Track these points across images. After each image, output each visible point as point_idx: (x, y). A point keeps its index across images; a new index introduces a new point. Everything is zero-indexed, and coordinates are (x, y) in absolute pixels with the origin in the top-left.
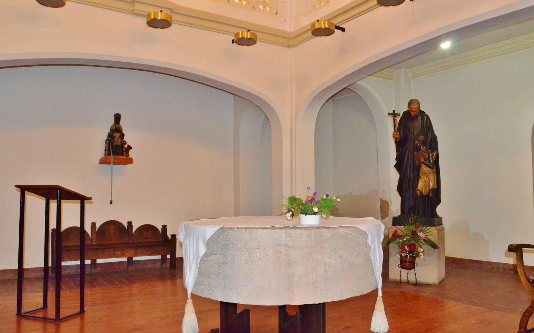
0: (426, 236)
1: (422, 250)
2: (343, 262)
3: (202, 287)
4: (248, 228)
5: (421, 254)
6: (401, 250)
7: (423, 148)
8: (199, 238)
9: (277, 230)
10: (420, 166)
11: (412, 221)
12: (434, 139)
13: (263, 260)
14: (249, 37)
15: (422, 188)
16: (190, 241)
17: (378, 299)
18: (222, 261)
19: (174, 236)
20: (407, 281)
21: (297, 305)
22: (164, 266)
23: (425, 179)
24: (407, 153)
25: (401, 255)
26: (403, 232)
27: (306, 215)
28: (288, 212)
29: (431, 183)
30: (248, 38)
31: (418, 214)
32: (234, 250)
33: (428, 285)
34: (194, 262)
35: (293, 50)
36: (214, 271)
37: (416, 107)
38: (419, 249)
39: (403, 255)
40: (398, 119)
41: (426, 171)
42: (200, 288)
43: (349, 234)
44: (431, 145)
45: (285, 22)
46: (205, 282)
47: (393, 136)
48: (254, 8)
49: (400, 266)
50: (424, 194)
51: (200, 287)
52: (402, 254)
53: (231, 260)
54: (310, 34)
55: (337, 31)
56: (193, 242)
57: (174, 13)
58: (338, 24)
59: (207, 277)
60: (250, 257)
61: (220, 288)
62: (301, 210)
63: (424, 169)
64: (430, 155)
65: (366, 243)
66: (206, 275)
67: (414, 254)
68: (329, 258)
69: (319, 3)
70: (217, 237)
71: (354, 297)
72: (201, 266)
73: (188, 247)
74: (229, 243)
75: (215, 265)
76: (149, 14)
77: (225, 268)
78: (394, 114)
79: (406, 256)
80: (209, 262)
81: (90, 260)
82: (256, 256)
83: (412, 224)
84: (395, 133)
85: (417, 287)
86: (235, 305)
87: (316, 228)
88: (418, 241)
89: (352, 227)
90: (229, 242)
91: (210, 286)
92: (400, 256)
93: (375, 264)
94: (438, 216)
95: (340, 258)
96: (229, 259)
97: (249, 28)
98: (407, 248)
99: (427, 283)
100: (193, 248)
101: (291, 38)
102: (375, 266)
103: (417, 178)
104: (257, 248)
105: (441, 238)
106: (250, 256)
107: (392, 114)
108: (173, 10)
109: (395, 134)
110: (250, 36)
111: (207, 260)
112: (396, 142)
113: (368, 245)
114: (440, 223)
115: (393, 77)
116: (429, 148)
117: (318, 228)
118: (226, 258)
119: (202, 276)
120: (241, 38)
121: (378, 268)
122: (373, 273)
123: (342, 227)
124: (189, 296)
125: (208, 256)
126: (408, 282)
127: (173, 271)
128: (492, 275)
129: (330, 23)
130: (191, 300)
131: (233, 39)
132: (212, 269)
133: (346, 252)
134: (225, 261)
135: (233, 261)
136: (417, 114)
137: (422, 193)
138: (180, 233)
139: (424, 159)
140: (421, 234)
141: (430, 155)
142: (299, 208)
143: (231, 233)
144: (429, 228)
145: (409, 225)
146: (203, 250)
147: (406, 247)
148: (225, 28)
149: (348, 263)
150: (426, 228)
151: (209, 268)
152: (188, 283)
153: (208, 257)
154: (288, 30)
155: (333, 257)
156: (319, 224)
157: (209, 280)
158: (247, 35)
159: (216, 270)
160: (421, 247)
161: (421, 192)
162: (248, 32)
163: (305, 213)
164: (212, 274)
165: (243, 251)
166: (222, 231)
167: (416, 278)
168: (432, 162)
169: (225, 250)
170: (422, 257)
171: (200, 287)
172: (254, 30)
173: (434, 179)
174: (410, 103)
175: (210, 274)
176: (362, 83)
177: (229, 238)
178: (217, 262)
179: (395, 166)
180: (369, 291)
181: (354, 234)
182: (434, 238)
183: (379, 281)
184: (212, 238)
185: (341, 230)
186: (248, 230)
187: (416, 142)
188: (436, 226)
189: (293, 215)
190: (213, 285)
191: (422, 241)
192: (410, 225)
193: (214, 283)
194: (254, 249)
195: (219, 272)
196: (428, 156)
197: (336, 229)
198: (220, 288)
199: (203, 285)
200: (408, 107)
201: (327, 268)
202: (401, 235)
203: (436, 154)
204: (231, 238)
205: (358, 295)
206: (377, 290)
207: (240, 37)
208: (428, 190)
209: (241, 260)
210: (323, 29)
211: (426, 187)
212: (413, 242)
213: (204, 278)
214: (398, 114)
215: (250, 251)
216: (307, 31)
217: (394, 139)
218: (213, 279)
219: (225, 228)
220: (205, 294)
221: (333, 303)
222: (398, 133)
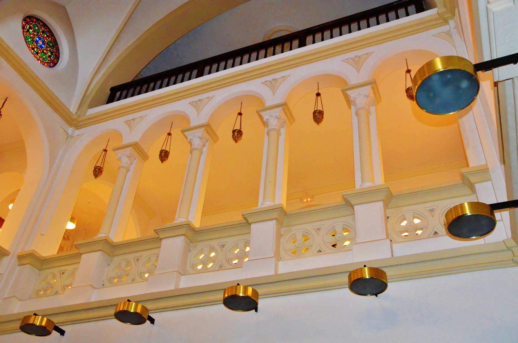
21: (326, 41)
55: (55, 333)
81: (494, 211)
128: (333, 227)
148: (330, 281)
210: (130, 312)
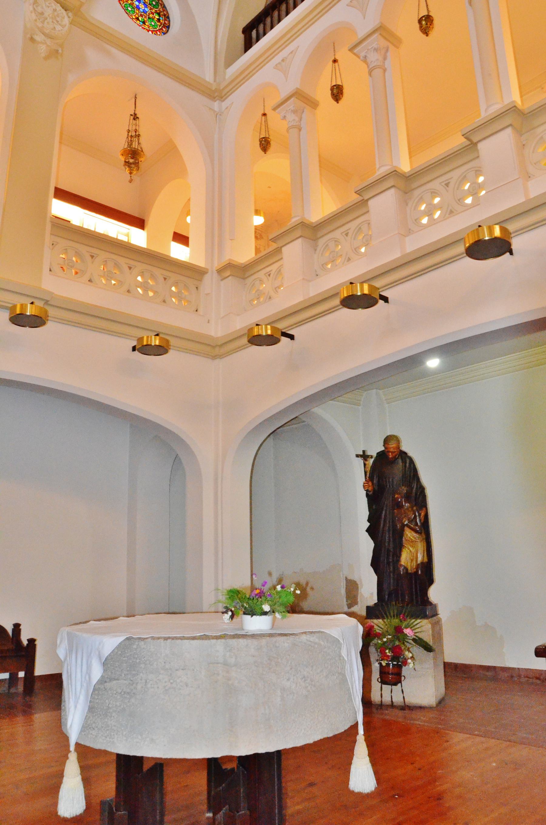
0: (415, 633)
1: (410, 655)
2: (307, 685)
3: (94, 733)
4: (169, 638)
5: (409, 661)
6: (380, 656)
7: (406, 505)
8: (92, 655)
9: (212, 640)
10: (402, 530)
11: (394, 612)
12: (421, 490)
13: (192, 687)
14: (157, 343)
15: (406, 562)
16: (76, 658)
17: (358, 740)
18: (128, 690)
19: (32, 642)
20: (391, 703)
22: (13, 690)
23: (411, 549)
24: (384, 512)
25: (380, 664)
26: (382, 628)
27: (252, 616)
28: (226, 612)
29: (419, 555)
30: (155, 345)
31: (403, 601)
32: (146, 672)
33: (421, 708)
34: (83, 692)
35: (221, 363)
36: (114, 706)
37: (394, 445)
38: (407, 653)
39: (384, 663)
40: (371, 461)
41: (412, 538)
42: (91, 734)
43: (315, 643)
44: (416, 499)
45: (209, 322)
46: (100, 723)
47: (364, 488)
48: (164, 301)
49: (379, 680)
50: (410, 571)
51: (91, 732)
52: (382, 662)
53: (142, 687)
54: (245, 340)
55: (284, 339)
56: (82, 660)
57: (50, 305)
58: (285, 329)
59: (103, 715)
60: (171, 683)
61: (124, 733)
62: (245, 608)
63: (409, 535)
64: (417, 514)
65: (340, 656)
66: (101, 713)
67: (399, 662)
68: (288, 680)
69: (258, 299)
70: (120, 652)
71: (325, 739)
72: (94, 698)
73: (73, 668)
74: (140, 662)
75: (116, 696)
76: (15, 306)
77: (133, 700)
78: (364, 456)
79: (388, 665)
80: (107, 692)
82: (181, 681)
83: (394, 616)
84: (366, 483)
85: (407, 712)
86: (141, 758)
87: (269, 636)
88: (404, 642)
89: (319, 632)
90: (139, 661)
91: (107, 730)
92: (379, 665)
93: (352, 686)
94: (431, 604)
95: (304, 679)
96: (139, 687)
97: (159, 330)
98: (389, 652)
99: (419, 705)
100: (82, 670)
101: (217, 345)
102: (352, 688)
103: (399, 547)
104: (182, 669)
105: (438, 635)
106: (171, 681)
107: (361, 456)
108: (48, 301)
109: (366, 484)
110: (159, 342)
111: (104, 688)
112: (367, 495)
113: (342, 658)
114: (435, 614)
115: (360, 401)
116: (414, 503)
117: (271, 635)
118: (134, 685)
119: (94, 715)
120: (146, 345)
121: (357, 692)
122: (350, 699)
123: (305, 633)
124: (72, 748)
125: (106, 682)
126: (392, 705)
127: (28, 698)
129: (273, 328)
130: (76, 754)
131: (77, 275)
132: (111, 702)
133: (312, 670)
134: (132, 690)
135: (145, 690)
136: (396, 455)
137: (407, 569)
138: (59, 646)
139: (408, 520)
140: (407, 631)
141: (417, 514)
142: (243, 606)
143: (143, 647)
144: (419, 621)
145: (390, 618)
146: (97, 673)
147: (387, 651)
149: (314, 686)
150: (414, 622)
151: (107, 701)
152: (71, 725)
153: (105, 684)
154: (213, 334)
155: (294, 679)
156: (271, 629)
157: (106, 720)
158: (156, 342)
159: (118, 704)
160: (408, 650)
161: (406, 569)
162: (157, 337)
163: (250, 613)
164: (111, 711)
165: (160, 674)
166: (128, 643)
167: (404, 698)
168: (419, 524)
169: (134, 672)
170: (411, 665)
171: (91, 732)
172: (165, 334)
173: (423, 549)
174: (386, 441)
175: (108, 711)
176: (318, 410)
177: (139, 654)
178: (120, 691)
179: (367, 531)
180: (346, 728)
181: (322, 643)
182: (427, 637)
183: (359, 711)
184: (112, 654)
185: (304, 638)
186: (169, 641)
187: (396, 496)
188: (429, 618)
189: (232, 617)
190: (113, 728)
191: (411, 641)
192: (391, 617)
193: (115, 726)
194: (177, 670)
195: (122, 707)
196: (413, 516)
197: (297, 637)
198: (124, 733)
199: (96, 729)
200: (384, 446)
201: (285, 696)
202: (379, 633)
203: (425, 513)
204: (143, 654)
205: (331, 735)
206: (357, 724)
207: (145, 343)
208: (415, 564)
209: (158, 688)
211: (412, 560)
212: (397, 643)
213: (98, 717)
214: (370, 457)
215: (171, 674)
216: (240, 337)
217: (365, 492)
218: (112, 718)
219: (133, 638)
220: (99, 744)
221: (294, 749)
222: (370, 483)
